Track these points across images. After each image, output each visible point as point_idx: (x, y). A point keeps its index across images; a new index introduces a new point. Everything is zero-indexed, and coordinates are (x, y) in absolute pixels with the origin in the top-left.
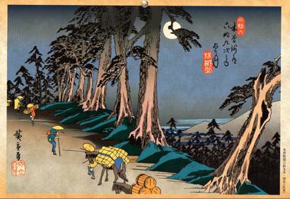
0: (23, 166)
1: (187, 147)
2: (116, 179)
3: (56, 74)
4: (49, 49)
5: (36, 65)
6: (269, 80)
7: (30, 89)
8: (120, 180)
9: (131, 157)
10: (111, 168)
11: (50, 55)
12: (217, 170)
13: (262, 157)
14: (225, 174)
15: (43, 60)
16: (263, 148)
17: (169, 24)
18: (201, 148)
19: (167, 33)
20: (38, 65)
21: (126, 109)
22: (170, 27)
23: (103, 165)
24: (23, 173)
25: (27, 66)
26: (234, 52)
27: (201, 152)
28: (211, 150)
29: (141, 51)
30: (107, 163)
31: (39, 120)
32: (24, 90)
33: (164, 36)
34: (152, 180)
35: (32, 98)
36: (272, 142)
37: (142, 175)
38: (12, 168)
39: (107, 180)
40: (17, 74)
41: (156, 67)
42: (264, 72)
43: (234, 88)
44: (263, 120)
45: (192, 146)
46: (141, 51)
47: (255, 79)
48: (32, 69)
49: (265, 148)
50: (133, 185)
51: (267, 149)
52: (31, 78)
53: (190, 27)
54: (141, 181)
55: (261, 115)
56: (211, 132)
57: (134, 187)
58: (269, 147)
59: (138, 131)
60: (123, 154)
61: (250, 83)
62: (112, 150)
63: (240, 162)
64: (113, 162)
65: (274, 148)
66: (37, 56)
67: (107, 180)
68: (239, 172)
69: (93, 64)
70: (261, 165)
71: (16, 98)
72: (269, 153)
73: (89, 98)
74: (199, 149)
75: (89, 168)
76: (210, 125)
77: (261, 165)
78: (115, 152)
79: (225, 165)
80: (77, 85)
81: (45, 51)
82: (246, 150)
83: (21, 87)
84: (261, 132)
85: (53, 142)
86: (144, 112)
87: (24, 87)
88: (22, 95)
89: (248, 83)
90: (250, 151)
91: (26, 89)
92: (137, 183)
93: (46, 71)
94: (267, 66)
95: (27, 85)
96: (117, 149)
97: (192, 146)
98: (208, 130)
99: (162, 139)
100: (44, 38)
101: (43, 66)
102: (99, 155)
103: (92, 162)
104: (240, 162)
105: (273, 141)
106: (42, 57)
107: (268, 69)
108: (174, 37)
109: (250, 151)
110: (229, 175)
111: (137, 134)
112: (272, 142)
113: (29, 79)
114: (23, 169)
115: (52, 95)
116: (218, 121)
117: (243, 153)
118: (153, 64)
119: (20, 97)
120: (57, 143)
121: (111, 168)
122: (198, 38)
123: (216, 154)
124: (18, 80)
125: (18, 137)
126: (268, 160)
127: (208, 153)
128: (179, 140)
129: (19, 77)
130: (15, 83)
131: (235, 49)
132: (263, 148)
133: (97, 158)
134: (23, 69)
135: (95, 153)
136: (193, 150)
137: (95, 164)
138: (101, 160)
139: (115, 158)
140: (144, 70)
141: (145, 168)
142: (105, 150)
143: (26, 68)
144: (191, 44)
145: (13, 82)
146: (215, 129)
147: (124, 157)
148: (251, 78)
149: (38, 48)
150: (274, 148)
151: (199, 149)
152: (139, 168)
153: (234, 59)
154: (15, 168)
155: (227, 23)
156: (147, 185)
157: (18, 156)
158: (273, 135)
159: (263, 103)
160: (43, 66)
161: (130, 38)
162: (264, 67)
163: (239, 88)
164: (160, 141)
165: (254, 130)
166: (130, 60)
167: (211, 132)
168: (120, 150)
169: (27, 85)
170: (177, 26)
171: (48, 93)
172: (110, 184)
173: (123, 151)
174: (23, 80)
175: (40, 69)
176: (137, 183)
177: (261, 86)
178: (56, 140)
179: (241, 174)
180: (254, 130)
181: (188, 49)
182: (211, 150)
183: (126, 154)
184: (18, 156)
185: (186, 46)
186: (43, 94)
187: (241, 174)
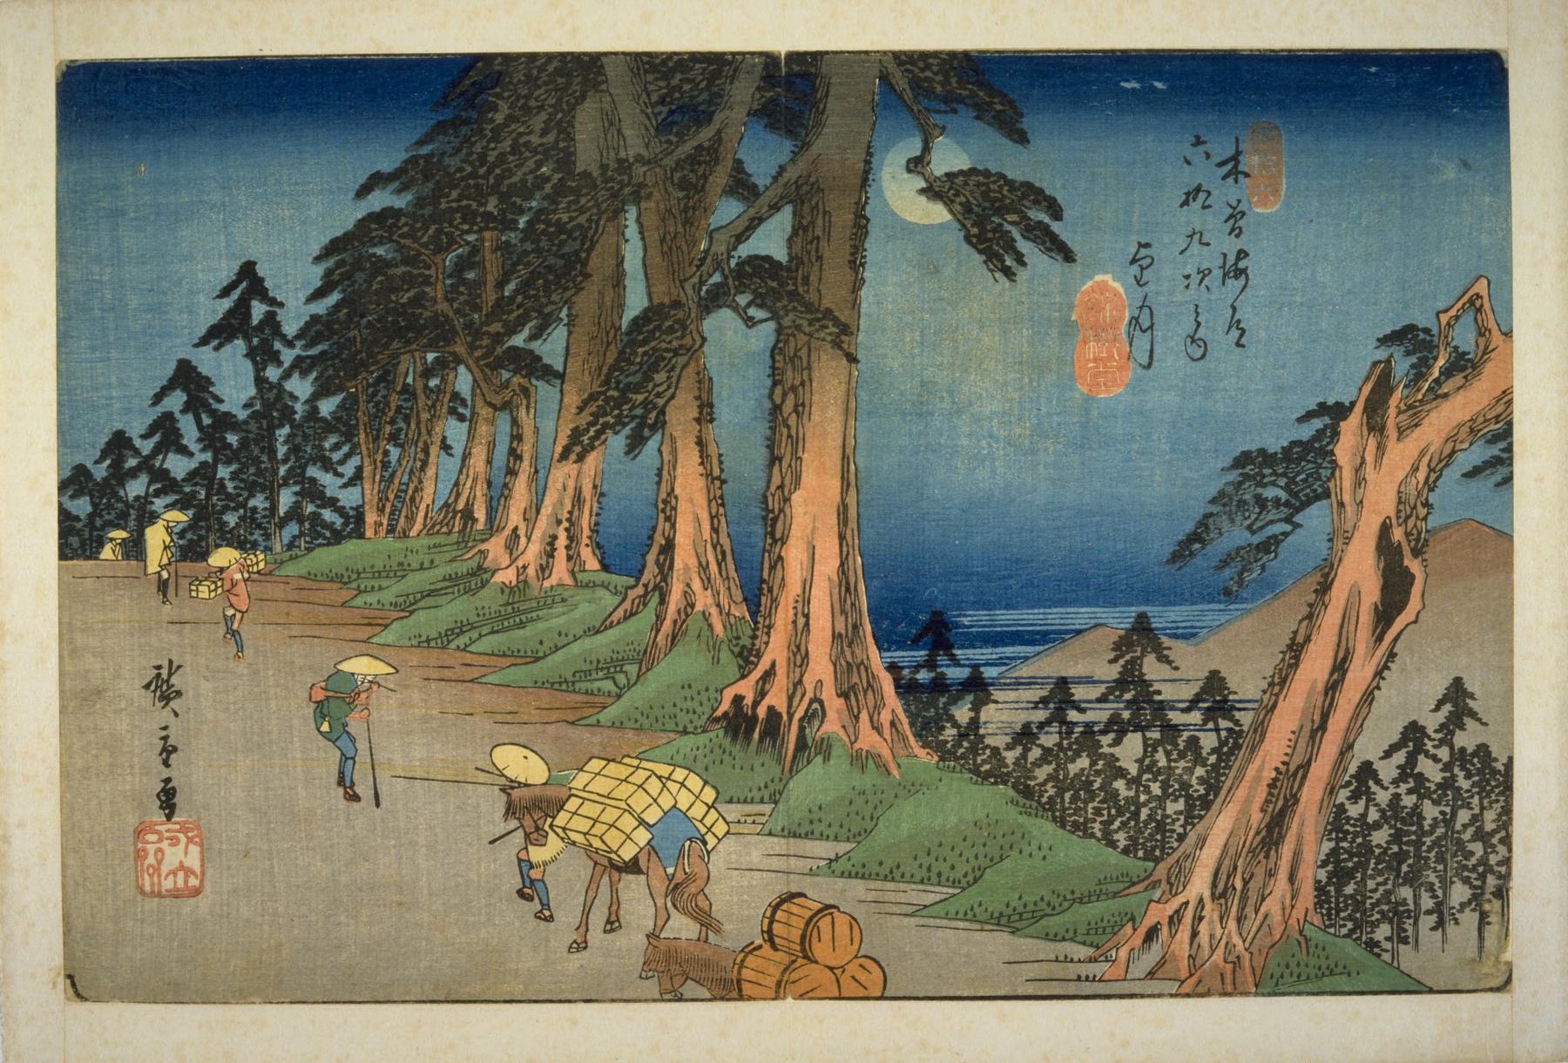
0: (194, 850)
1: (1010, 756)
2: (662, 919)
3: (354, 399)
4: (315, 275)
5: (251, 354)
6: (1414, 414)
7: (223, 472)
8: (682, 927)
9: (733, 812)
10: (633, 867)
11: (321, 307)
12: (1161, 871)
13: (1383, 797)
14: (1199, 885)
15: (290, 328)
16: (1388, 754)
17: (914, 147)
18: (1083, 762)
19: (901, 197)
20: (262, 355)
21: (704, 567)
22: (916, 164)
23: (589, 850)
24: (193, 882)
25: (206, 361)
26: (1234, 285)
27: (1083, 784)
28: (1133, 770)
29: (768, 284)
30: (613, 839)
31: (1294, 826)
32: (192, 475)
33: (887, 205)
34: (842, 922)
35: (231, 519)
36: (1432, 722)
37: (792, 896)
38: (140, 855)
39: (613, 924)
40: (158, 398)
41: (852, 359)
42: (1383, 387)
43: (1243, 460)
44: (1387, 613)
45: (1035, 753)
46: (768, 284)
47: (1339, 412)
48: (233, 379)
49: (1400, 757)
50: (750, 949)
51: (1412, 760)
52: (225, 421)
53: (1015, 163)
54: (789, 929)
55: (1371, 592)
56: (1131, 679)
57: (751, 961)
58: (1419, 749)
59: (769, 674)
60: (690, 794)
61: (1320, 433)
62: (640, 776)
63: (1273, 832)
64: (642, 836)
65: (1444, 754)
66: (258, 310)
67: (613, 924)
68: (1271, 874)
69: (535, 346)
70: (1380, 837)
71: (153, 517)
72: (1420, 779)
73: (515, 518)
74: (1073, 768)
75: (524, 865)
76: (1122, 646)
77: (1380, 837)
78: (654, 786)
79: (1202, 842)
80: (458, 449)
81: (296, 293)
82: (1306, 766)
83: (178, 466)
84: (1379, 674)
85: (339, 735)
86: (794, 588)
87: (193, 464)
88: (181, 505)
89: (1306, 432)
90: (1321, 770)
91: (203, 474)
92: (769, 936)
93: (301, 387)
94: (1397, 351)
95: (208, 457)
96: (664, 770)
97: (1035, 753)
98: (1113, 672)
99: (885, 717)
100: (289, 217)
101: (288, 356)
102: (572, 805)
103: (535, 836)
104: (1273, 832)
105: (1441, 716)
106: (281, 315)
107: (1402, 366)
108: (938, 213)
109: (1321, 770)
110: (1220, 893)
111: (761, 694)
112: (1432, 722)
113: (217, 428)
114: (193, 860)
115: (332, 503)
116: (1163, 617)
117: (1289, 780)
118: (837, 344)
119: (179, 517)
120: (362, 746)
121: (633, 867)
122: (1057, 214)
123: (1156, 789)
124: (165, 428)
125: (166, 699)
126: (1416, 811)
127: (1120, 785)
128: (974, 723)
129: (168, 417)
130: (146, 447)
131: (1240, 273)
132: (1388, 754)
133: (562, 818)
134: (187, 377)
135: (550, 792)
136: (1042, 773)
137: (554, 844)
138: (584, 825)
139: (652, 816)
140: (790, 377)
141: (805, 865)
142: (595, 779)
143: (204, 370)
144: (1023, 246)
145: (138, 442)
146: (1151, 668)
147: (698, 811)
148: (1323, 409)
149: (261, 270)
150: (1444, 754)
151: (1073, 768)
152: (1088, 988)
153: (1235, 323)
154: (151, 860)
155: (1198, 142)
156: (820, 950)
157: (168, 799)
158: (1440, 692)
159: (1385, 529)
160: (288, 356)
161: (716, 220)
162: (1382, 354)
163: (1266, 457)
164: (877, 729)
165: (1340, 667)
166: (722, 327)
167: (1131, 679)
168: (680, 774)
169: (208, 457)
170: (949, 158)
171: (312, 491)
172: (632, 941)
173: (695, 782)
174: (189, 430)
175: (272, 373)
176: (769, 936)
177: (1372, 444)
178: (355, 726)
179: (1281, 885)
180: (1340, 667)
181: (1009, 273)
182: (1133, 770)
183: (709, 795)
184: (168, 799)
185: (995, 250)
186: (286, 499)
187: (1281, 885)
